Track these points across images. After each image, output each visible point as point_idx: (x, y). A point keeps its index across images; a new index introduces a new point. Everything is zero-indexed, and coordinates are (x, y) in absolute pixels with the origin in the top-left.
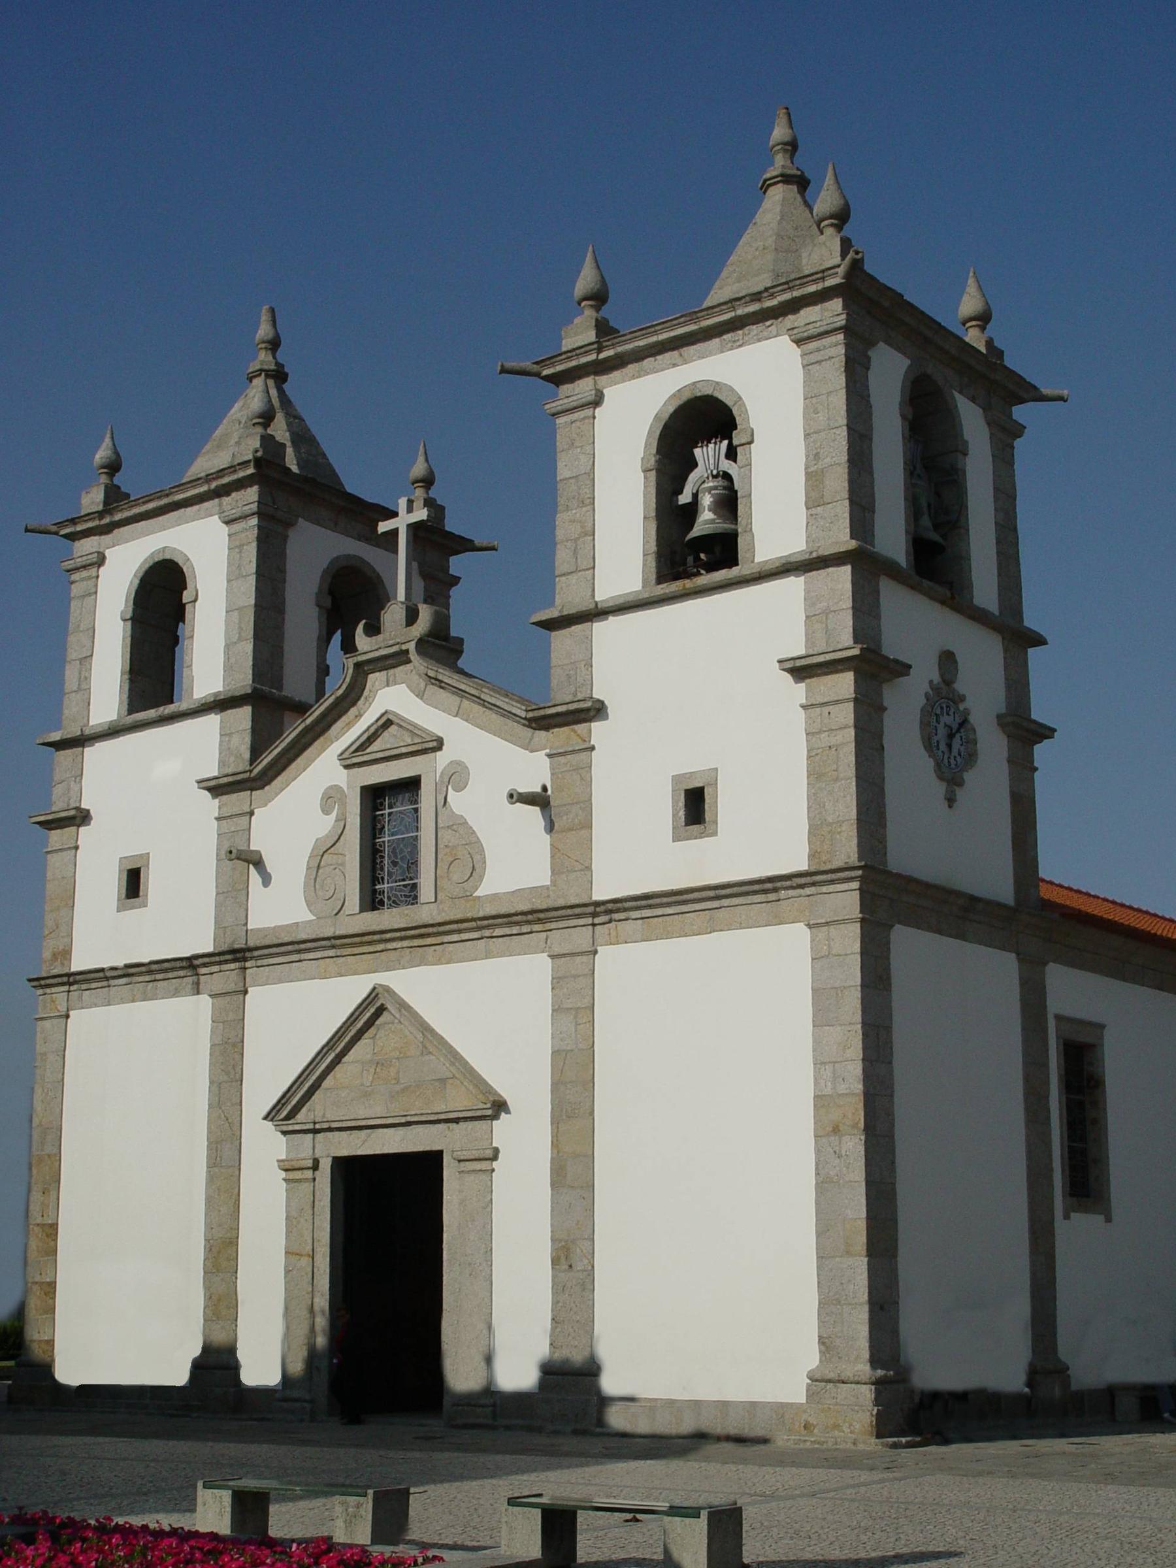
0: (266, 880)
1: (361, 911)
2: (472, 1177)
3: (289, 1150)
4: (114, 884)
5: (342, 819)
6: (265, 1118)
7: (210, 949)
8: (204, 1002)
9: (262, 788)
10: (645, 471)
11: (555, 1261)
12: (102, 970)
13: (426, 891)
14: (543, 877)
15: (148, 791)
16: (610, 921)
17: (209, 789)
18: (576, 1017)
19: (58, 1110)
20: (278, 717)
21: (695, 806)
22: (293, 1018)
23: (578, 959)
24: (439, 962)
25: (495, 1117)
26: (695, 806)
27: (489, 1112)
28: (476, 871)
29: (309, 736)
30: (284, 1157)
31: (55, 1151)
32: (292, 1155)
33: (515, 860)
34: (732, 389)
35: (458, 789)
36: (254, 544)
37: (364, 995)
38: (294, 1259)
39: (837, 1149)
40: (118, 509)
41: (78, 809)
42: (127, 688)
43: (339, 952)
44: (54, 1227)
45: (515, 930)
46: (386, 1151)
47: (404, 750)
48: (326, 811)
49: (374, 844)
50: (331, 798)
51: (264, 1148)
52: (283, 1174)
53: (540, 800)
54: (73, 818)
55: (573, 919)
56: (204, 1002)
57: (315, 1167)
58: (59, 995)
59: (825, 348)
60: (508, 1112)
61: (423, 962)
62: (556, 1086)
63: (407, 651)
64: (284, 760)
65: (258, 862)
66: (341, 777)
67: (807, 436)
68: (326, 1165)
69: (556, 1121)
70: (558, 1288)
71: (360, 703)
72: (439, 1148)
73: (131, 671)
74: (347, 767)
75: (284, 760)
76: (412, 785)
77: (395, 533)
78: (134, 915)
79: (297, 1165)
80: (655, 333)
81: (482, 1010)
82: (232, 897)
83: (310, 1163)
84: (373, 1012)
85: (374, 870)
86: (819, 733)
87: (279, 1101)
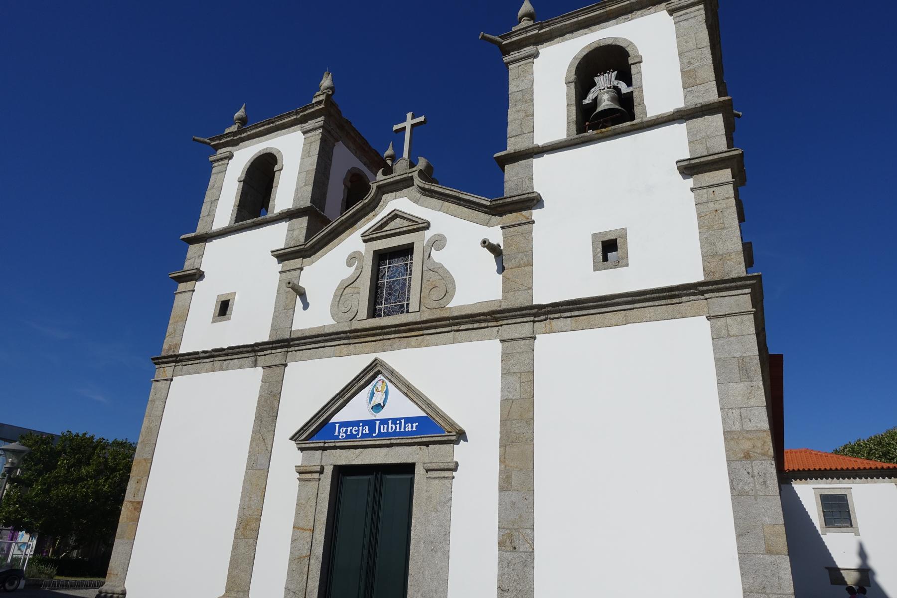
0: (306, 306)
1: (368, 317)
2: (437, 481)
3: (304, 459)
4: (212, 307)
5: (360, 269)
6: (291, 439)
7: (267, 339)
8: (259, 371)
9: (310, 256)
10: (568, 83)
11: (501, 544)
12: (197, 353)
13: (414, 305)
14: (498, 296)
15: (237, 274)
16: (546, 320)
17: (277, 257)
18: (520, 378)
19: (160, 408)
20: (320, 224)
21: (609, 248)
22: (311, 383)
23: (523, 342)
24: (419, 346)
25: (456, 442)
26: (609, 248)
27: (454, 438)
28: (448, 293)
29: (343, 227)
30: (300, 464)
31: (150, 457)
32: (306, 464)
33: (477, 284)
34: (626, 40)
35: (437, 249)
36: (319, 142)
37: (368, 364)
38: (298, 532)
39: (750, 470)
40: (245, 131)
41: (198, 269)
42: (236, 212)
43: (351, 341)
44: (140, 503)
45: (476, 326)
46: (373, 462)
47: (404, 229)
48: (349, 264)
49: (377, 284)
50: (352, 259)
51: (286, 457)
52: (297, 475)
53: (495, 250)
54: (194, 274)
55: (518, 317)
56: (259, 371)
57: (321, 472)
58: (168, 369)
59: (691, 12)
60: (466, 440)
61: (408, 346)
62: (504, 422)
63: (412, 178)
64: (326, 240)
65: (302, 294)
66: (362, 247)
67: (680, 54)
68: (329, 471)
69: (504, 445)
70: (503, 564)
71: (377, 209)
72: (410, 461)
73: (239, 206)
74: (365, 241)
75: (326, 240)
76: (407, 251)
77: (404, 128)
78: (223, 324)
79: (308, 469)
80: (577, 16)
81: (455, 377)
82: (284, 311)
83: (318, 468)
84: (375, 363)
85: (376, 298)
86: (708, 202)
87: (302, 428)
